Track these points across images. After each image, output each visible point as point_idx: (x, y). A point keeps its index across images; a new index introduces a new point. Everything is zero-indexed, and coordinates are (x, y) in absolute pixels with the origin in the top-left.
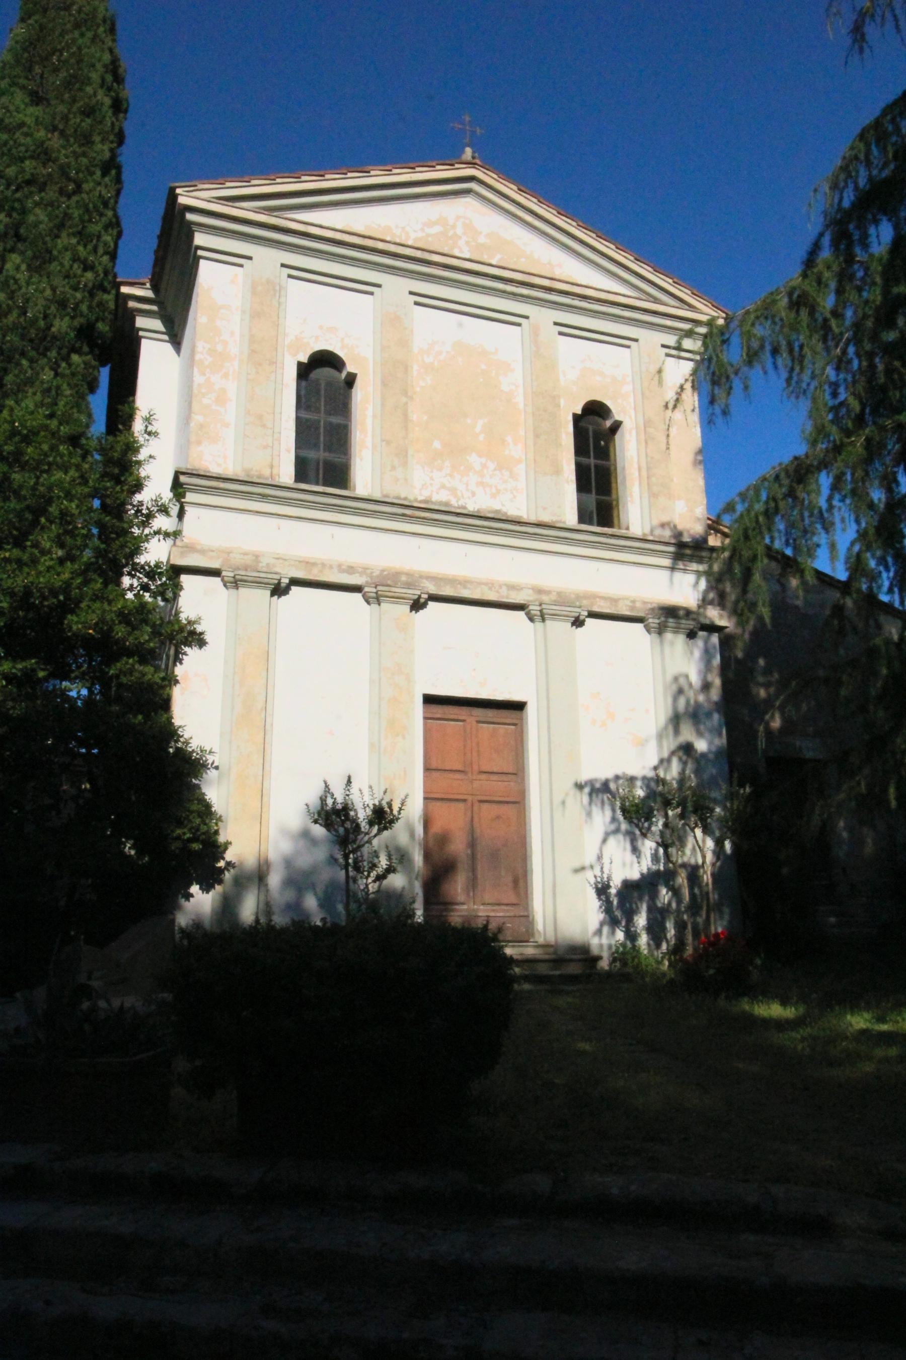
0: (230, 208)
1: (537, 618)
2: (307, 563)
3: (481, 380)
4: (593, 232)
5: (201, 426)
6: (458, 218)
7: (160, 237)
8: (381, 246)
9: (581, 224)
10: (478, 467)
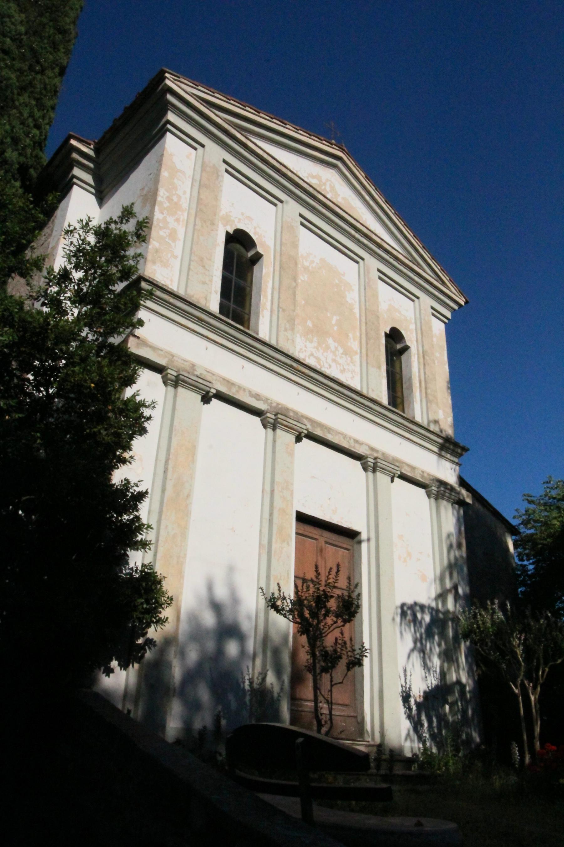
0: (199, 104)
1: (370, 469)
2: (228, 381)
3: (336, 290)
4: (403, 221)
5: (157, 251)
6: (327, 180)
7: (126, 109)
8: (290, 174)
9: (397, 213)
10: (333, 348)
